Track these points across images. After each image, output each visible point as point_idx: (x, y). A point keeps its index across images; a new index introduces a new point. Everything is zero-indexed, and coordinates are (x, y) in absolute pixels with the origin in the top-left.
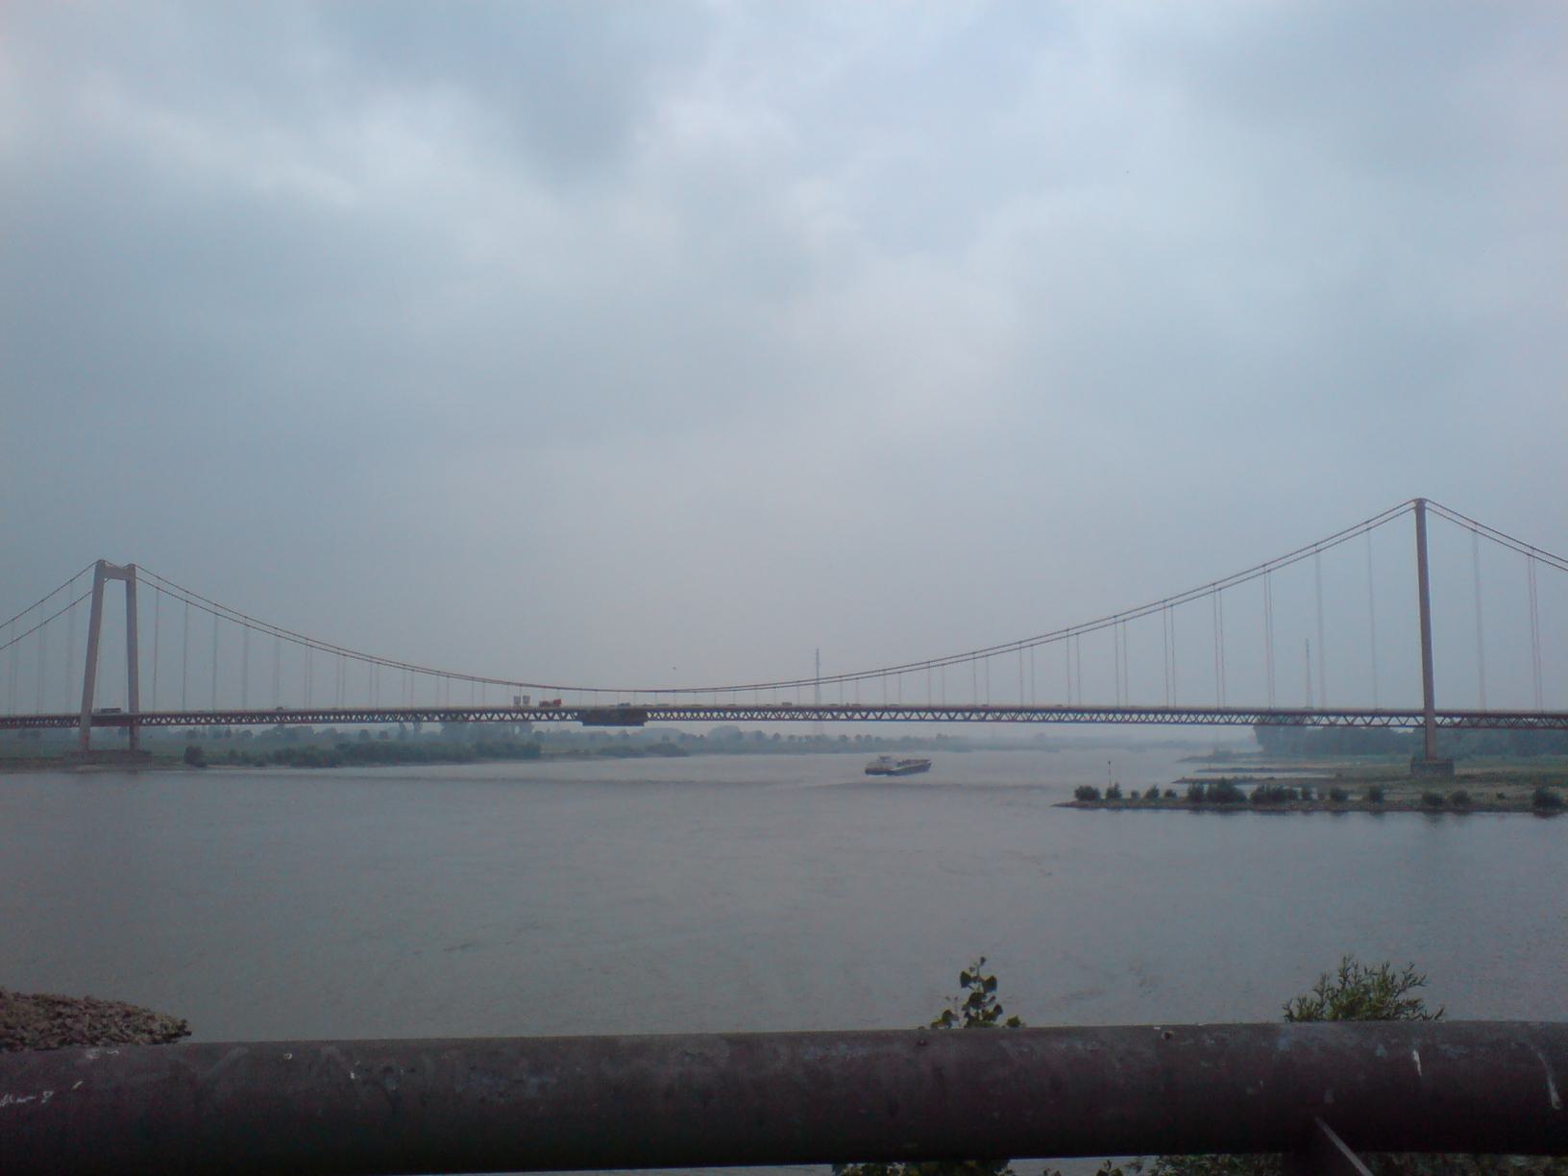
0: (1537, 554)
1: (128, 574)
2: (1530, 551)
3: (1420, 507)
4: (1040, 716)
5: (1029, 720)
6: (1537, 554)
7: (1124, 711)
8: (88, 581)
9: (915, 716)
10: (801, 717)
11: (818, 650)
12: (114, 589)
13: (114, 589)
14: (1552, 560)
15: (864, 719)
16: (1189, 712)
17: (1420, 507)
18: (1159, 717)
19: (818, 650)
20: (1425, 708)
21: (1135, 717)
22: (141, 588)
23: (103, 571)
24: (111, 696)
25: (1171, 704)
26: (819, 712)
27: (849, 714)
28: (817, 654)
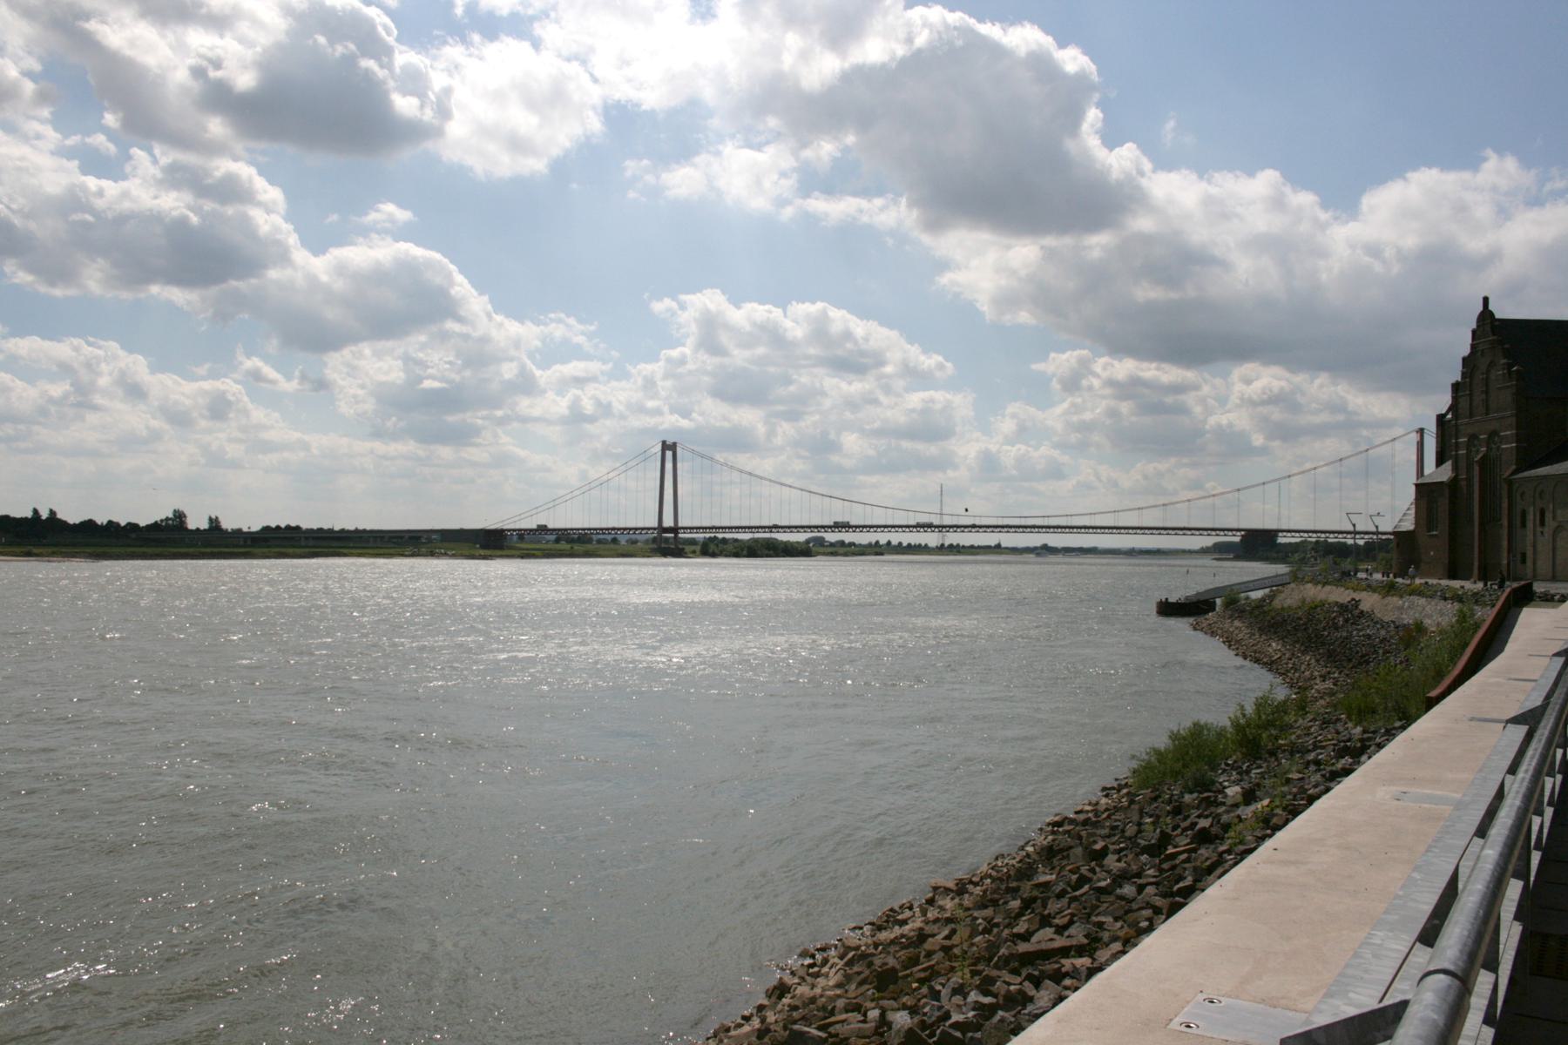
4: (1006, 529)
7: (1141, 528)
8: (659, 447)
12: (669, 454)
13: (669, 454)
22: (679, 450)
23: (666, 446)
24: (668, 522)
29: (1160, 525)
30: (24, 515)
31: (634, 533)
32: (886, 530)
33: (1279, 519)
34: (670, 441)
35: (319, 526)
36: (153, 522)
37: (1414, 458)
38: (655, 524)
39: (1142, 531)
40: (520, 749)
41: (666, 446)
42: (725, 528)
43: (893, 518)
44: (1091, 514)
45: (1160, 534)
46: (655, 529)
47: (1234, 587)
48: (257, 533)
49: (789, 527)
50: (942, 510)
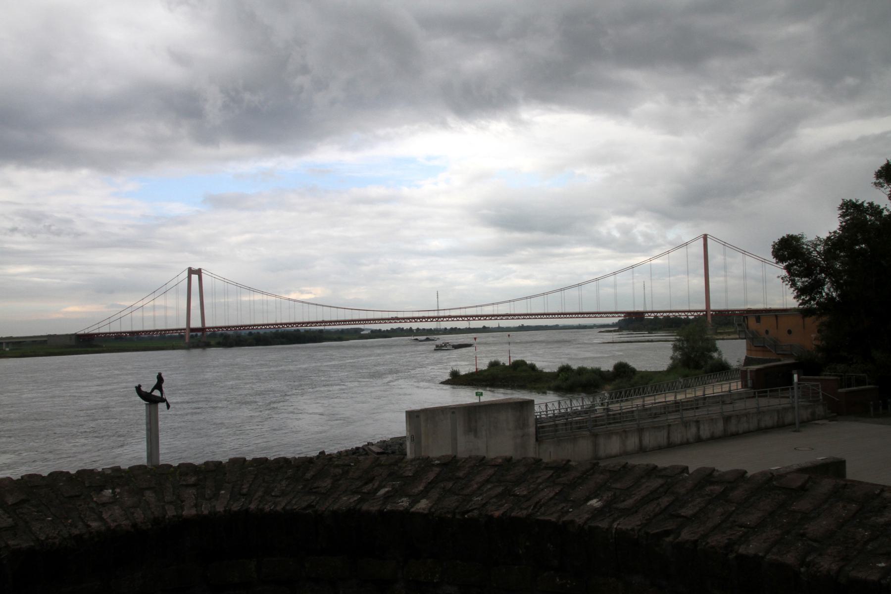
0: (726, 245)
1: (199, 272)
2: (724, 243)
3: (705, 237)
5: (507, 319)
6: (726, 245)
7: (546, 314)
8: (186, 274)
9: (455, 319)
10: (403, 321)
11: (437, 292)
12: (195, 278)
13: (195, 278)
14: (720, 241)
15: (426, 321)
16: (587, 313)
17: (705, 237)
18: (571, 316)
19: (437, 292)
20: (707, 308)
21: (568, 316)
23: (191, 271)
24: (196, 323)
25: (581, 311)
26: (437, 319)
27: (421, 320)
28: (437, 293)
29: (577, 311)
30: (495, 326)
31: (235, 329)
32: (450, 319)
33: (493, 311)
34: (195, 267)
35: (546, 324)
36: (429, 328)
37: (710, 279)
38: (703, 307)
39: (600, 315)
40: (275, 427)
41: (191, 271)
42: (356, 321)
43: (689, 306)
44: (510, 301)
45: (607, 317)
46: (184, 329)
47: (738, 337)
48: (602, 372)
49: (374, 320)
50: (438, 307)
